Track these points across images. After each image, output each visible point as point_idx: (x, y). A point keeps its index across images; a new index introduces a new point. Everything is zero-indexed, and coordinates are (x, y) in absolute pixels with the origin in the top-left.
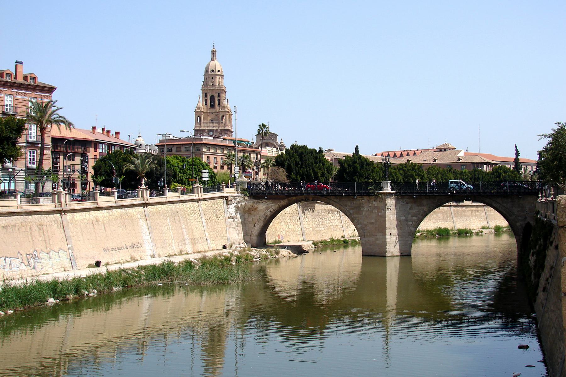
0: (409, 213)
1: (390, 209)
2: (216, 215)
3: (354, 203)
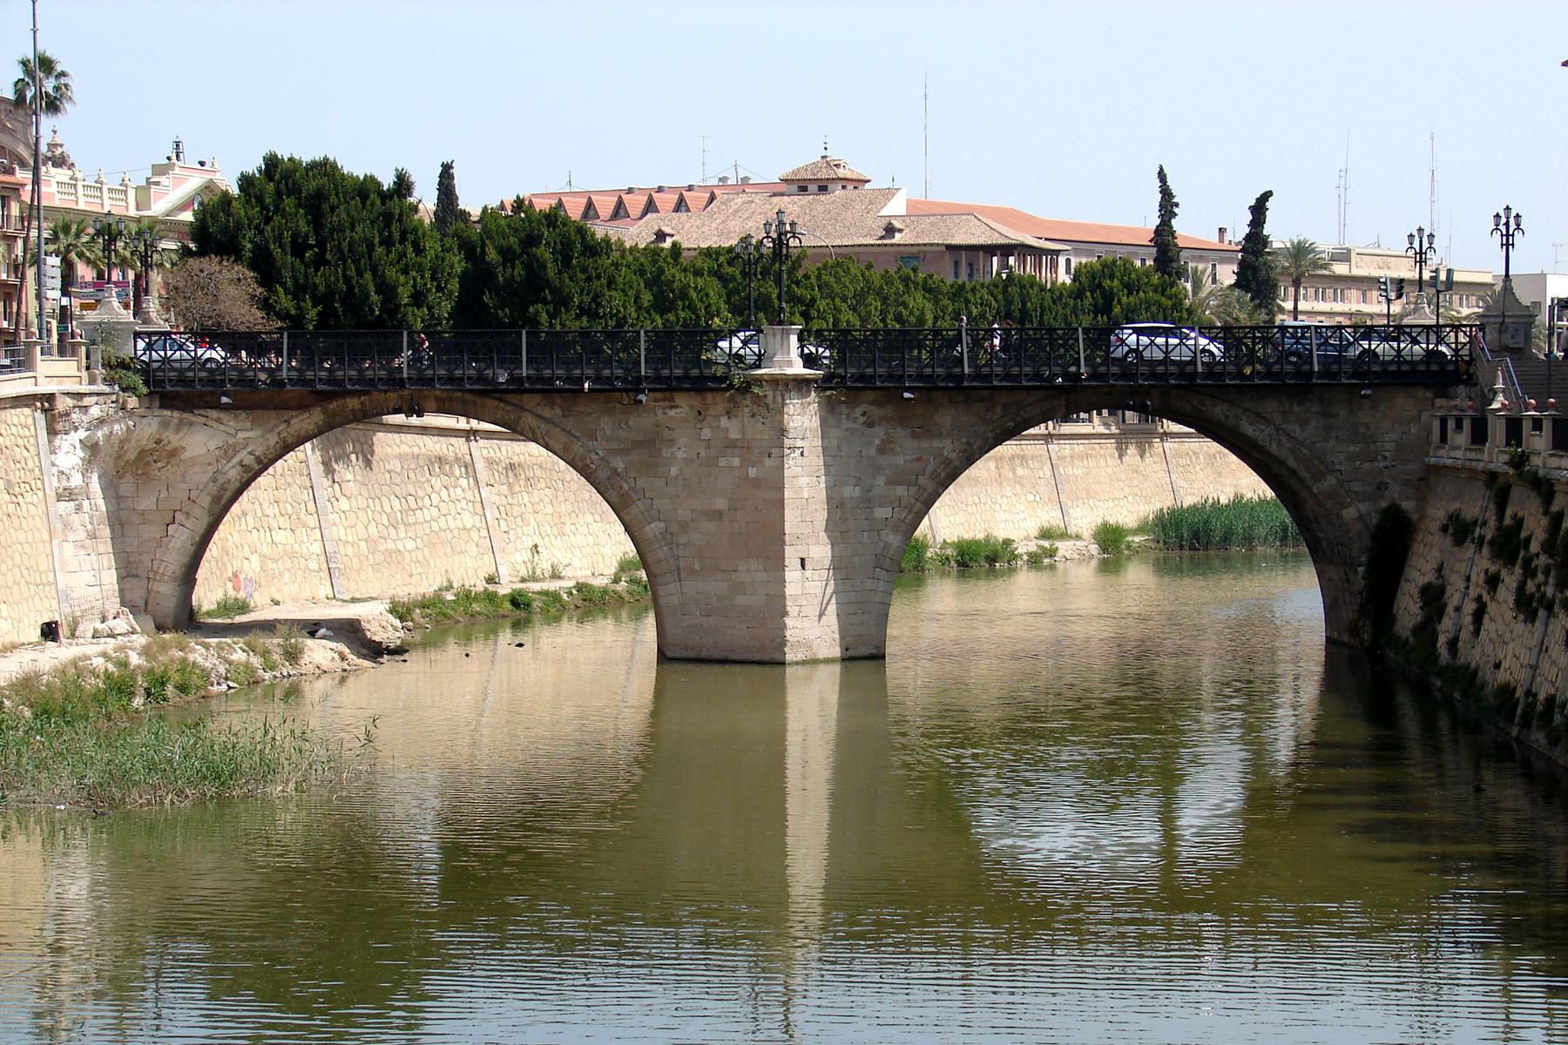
0: (877, 470)
1: (798, 452)
2: (9, 482)
3: (631, 423)
